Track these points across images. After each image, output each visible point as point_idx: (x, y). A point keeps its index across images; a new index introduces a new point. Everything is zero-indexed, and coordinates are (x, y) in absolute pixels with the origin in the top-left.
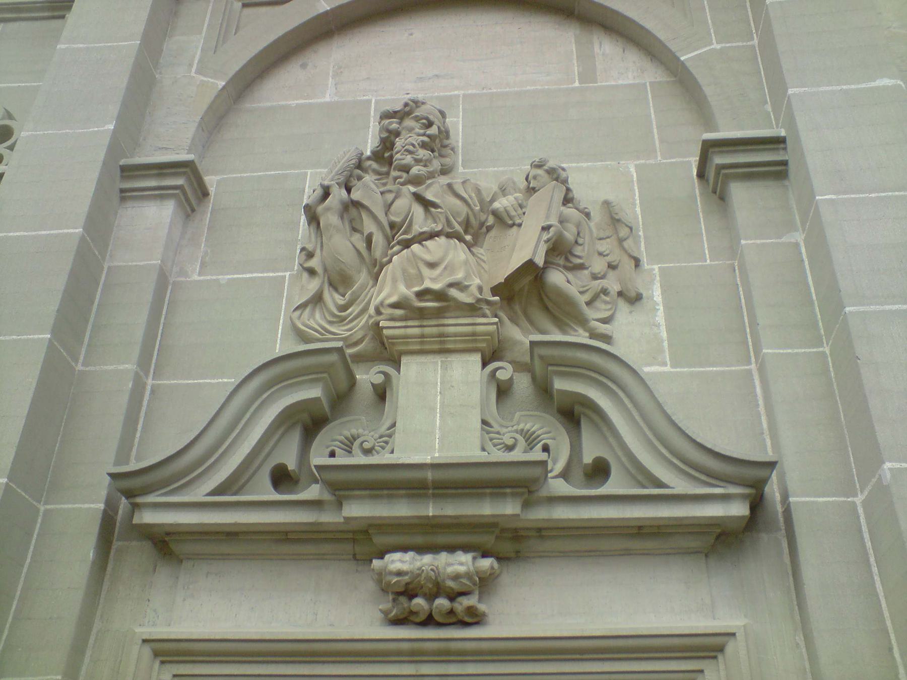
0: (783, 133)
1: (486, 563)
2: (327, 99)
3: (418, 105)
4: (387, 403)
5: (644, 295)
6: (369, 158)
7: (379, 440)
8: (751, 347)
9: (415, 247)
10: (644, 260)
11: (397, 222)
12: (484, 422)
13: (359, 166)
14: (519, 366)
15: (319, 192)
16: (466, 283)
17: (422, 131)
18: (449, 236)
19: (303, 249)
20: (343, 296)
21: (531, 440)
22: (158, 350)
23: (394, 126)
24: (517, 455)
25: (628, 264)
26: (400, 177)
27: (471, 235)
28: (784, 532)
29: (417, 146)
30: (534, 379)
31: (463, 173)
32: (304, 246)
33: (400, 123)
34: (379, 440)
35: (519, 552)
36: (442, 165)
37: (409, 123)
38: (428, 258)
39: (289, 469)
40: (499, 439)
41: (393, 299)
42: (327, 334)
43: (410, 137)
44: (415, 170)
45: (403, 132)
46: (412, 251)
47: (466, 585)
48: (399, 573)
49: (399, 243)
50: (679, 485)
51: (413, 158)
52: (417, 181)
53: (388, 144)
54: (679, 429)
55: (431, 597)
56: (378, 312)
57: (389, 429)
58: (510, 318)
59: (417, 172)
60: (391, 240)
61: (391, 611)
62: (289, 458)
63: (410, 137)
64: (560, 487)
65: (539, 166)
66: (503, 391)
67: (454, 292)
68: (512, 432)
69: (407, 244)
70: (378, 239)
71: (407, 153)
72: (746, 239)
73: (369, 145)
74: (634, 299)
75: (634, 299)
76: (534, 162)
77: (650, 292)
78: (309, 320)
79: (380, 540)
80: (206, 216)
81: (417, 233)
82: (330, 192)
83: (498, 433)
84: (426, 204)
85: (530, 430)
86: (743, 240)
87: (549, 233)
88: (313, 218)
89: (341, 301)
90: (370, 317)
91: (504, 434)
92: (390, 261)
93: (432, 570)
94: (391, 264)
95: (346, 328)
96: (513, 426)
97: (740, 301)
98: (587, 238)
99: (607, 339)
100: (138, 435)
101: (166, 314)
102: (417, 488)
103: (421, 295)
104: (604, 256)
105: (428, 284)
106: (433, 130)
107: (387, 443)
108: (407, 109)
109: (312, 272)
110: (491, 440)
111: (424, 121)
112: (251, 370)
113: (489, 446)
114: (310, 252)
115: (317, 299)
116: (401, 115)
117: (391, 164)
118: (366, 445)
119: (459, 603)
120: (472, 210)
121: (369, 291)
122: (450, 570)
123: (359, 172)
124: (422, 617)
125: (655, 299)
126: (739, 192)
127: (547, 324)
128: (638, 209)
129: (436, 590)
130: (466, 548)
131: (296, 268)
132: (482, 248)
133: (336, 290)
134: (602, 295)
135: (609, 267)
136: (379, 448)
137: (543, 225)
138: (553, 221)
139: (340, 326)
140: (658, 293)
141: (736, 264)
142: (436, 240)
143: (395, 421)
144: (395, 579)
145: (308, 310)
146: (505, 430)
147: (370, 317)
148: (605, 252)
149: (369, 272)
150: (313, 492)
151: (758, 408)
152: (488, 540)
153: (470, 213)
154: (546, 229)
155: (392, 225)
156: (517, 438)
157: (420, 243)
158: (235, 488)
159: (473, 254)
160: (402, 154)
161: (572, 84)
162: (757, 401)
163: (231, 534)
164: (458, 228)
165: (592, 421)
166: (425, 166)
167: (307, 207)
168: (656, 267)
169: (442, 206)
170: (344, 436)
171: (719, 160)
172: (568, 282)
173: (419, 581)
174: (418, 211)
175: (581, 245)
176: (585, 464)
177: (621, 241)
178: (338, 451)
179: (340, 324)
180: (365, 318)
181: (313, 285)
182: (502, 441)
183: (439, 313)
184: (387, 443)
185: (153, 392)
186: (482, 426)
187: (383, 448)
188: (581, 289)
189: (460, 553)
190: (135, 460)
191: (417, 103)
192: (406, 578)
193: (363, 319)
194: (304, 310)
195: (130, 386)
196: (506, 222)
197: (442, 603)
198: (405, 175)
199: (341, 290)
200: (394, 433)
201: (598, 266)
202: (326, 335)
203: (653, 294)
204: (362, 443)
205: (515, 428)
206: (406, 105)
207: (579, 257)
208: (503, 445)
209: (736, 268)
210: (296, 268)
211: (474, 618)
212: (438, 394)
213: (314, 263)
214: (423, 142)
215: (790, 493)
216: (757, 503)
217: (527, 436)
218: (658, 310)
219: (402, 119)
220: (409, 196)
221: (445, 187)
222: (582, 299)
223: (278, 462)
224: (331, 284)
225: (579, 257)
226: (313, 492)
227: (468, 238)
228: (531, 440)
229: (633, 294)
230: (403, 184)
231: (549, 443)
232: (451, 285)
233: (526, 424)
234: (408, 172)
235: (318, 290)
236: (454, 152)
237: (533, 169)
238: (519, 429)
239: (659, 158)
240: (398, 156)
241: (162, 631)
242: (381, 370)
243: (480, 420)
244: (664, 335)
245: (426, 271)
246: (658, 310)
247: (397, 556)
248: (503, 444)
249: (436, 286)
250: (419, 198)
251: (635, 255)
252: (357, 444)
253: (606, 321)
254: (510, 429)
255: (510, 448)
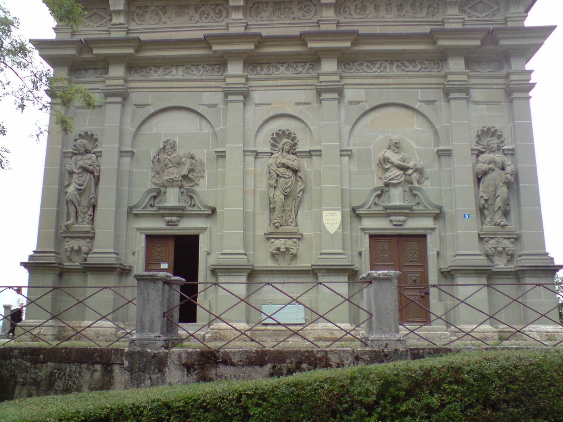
0: (451, 149)
2: (154, 132)
13: (160, 150)
25: (202, 171)
35: (354, 210)
37: (168, 144)
50: (203, 209)
62: (376, 201)
66: (182, 193)
67: (174, 179)
69: (168, 168)
73: (162, 146)
74: (203, 177)
75: (203, 177)
79: (164, 215)
80: (135, 158)
88: (153, 162)
102: (309, 85)
106: (172, 145)
116: (167, 142)
126: (219, 158)
127: (190, 183)
129: (172, 221)
130: (175, 216)
163: (145, 214)
174: (169, 162)
181: (154, 174)
183: (172, 182)
197: (173, 223)
211: (177, 225)
216: (441, 211)
241: (137, 227)
245: (170, 174)
249: (172, 178)
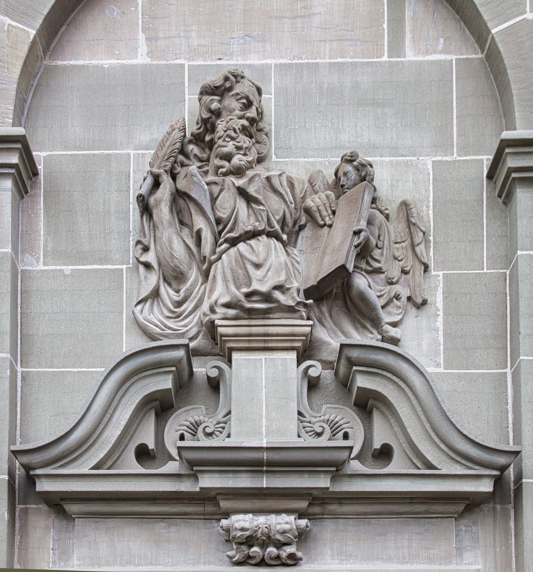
1: (303, 522)
3: (238, 79)
4: (221, 394)
5: (429, 301)
6: (190, 142)
7: (217, 426)
8: (509, 353)
9: (242, 246)
10: (432, 266)
11: (224, 218)
12: (300, 413)
13: (182, 151)
14: (326, 364)
15: (150, 181)
16: (287, 286)
17: (242, 113)
18: (270, 235)
19: (139, 242)
20: (178, 291)
21: (335, 429)
22: (21, 340)
23: (215, 106)
24: (323, 442)
26: (222, 167)
27: (286, 234)
28: (512, 504)
29: (238, 131)
30: (336, 374)
31: (276, 162)
32: (139, 239)
33: (220, 102)
34: (217, 426)
36: (258, 154)
38: (254, 259)
39: (150, 448)
40: (310, 427)
41: (225, 299)
42: (167, 329)
43: (231, 119)
44: (237, 160)
45: (224, 113)
46: (238, 249)
47: (290, 538)
48: (243, 529)
49: (226, 241)
51: (234, 145)
52: (238, 172)
53: (209, 126)
54: (451, 422)
55: (264, 545)
56: (212, 310)
57: (224, 417)
58: (318, 319)
59: (239, 162)
60: (217, 236)
61: (234, 557)
63: (231, 119)
64: (356, 466)
65: (350, 161)
67: (277, 295)
68: (320, 421)
69: (233, 242)
70: (207, 237)
71: (229, 139)
72: (522, 250)
76: (345, 155)
77: (434, 298)
78: (149, 315)
81: (243, 232)
82: (160, 181)
83: (310, 422)
84: (249, 199)
85: (333, 420)
86: (520, 250)
87: (359, 238)
89: (176, 298)
90: (205, 315)
91: (314, 424)
92: (220, 258)
93: (266, 527)
94: (221, 260)
95: (182, 323)
96: (320, 417)
97: (506, 310)
98: (386, 242)
99: (395, 341)
100: (19, 417)
101: (21, 303)
103: (248, 295)
104: (399, 261)
105: (256, 286)
106: (252, 113)
107: (223, 428)
108: (228, 85)
109: (147, 266)
110: (304, 428)
111: (244, 101)
112: (115, 363)
113: (303, 433)
114: (146, 246)
115: (155, 294)
117: (211, 148)
118: (208, 430)
119: (284, 550)
120: (288, 207)
121: (200, 289)
122: (278, 527)
123: (181, 158)
124: (258, 560)
125: (437, 305)
128: (431, 212)
130: (288, 512)
131: (131, 261)
132: (295, 247)
133: (170, 285)
134: (395, 300)
135: (402, 272)
136: (218, 432)
137: (354, 229)
138: (363, 224)
139: (176, 322)
140: (440, 299)
141: (508, 273)
142: (258, 239)
143: (229, 410)
144: (239, 534)
145: (148, 304)
146: (314, 420)
147: (205, 315)
148: (399, 256)
149: (199, 269)
150: (172, 467)
151: (507, 406)
152: (303, 504)
153: (286, 210)
154: (357, 233)
155: (218, 221)
156: (325, 427)
157: (244, 241)
158: (109, 464)
159: (288, 254)
160: (224, 140)
161: (380, 57)
162: (507, 399)
164: (277, 227)
165: (382, 413)
166: (245, 155)
167: (140, 197)
168: (441, 273)
169: (263, 202)
170: (189, 422)
171: (511, 162)
172: (370, 286)
173: (256, 536)
174: (242, 205)
175: (380, 249)
176: (375, 449)
177: (413, 246)
178: (187, 435)
179: (177, 320)
180: (199, 313)
182: (313, 429)
183: (264, 314)
184: (223, 428)
185: (23, 379)
186: (298, 417)
187: (221, 433)
188: (379, 294)
189: (284, 515)
190: (20, 438)
191: (238, 77)
192: (248, 533)
193: (196, 316)
194: (145, 304)
195: (9, 373)
196: (318, 222)
197: (272, 550)
198: (225, 163)
199: (174, 285)
200: (230, 419)
201: (395, 273)
202: (165, 330)
203: (436, 300)
204: (204, 429)
205: (322, 418)
206: (226, 79)
207: (378, 261)
208: (313, 432)
209: (508, 277)
210: (131, 261)
212: (264, 388)
213: (150, 257)
214: (243, 126)
215: (524, 473)
217: (331, 425)
218: (439, 315)
219: (222, 95)
220: (234, 190)
221: (264, 180)
222: (379, 303)
223: (139, 443)
224: (165, 280)
225: (378, 261)
226: (172, 467)
227: (285, 237)
228: (335, 429)
229: (419, 301)
230: (225, 174)
231: (348, 431)
232: (276, 288)
233: (331, 415)
234: (229, 161)
235: (155, 287)
236: (267, 137)
237: (344, 164)
238: (325, 419)
239: (455, 155)
240: (220, 142)
242: (216, 365)
243: (297, 412)
244: (441, 339)
246: (439, 315)
247: (241, 516)
248: (313, 431)
249: (264, 288)
250: (242, 192)
251: (425, 261)
252: (200, 429)
253: (394, 325)
254: (318, 419)
255: (319, 435)
